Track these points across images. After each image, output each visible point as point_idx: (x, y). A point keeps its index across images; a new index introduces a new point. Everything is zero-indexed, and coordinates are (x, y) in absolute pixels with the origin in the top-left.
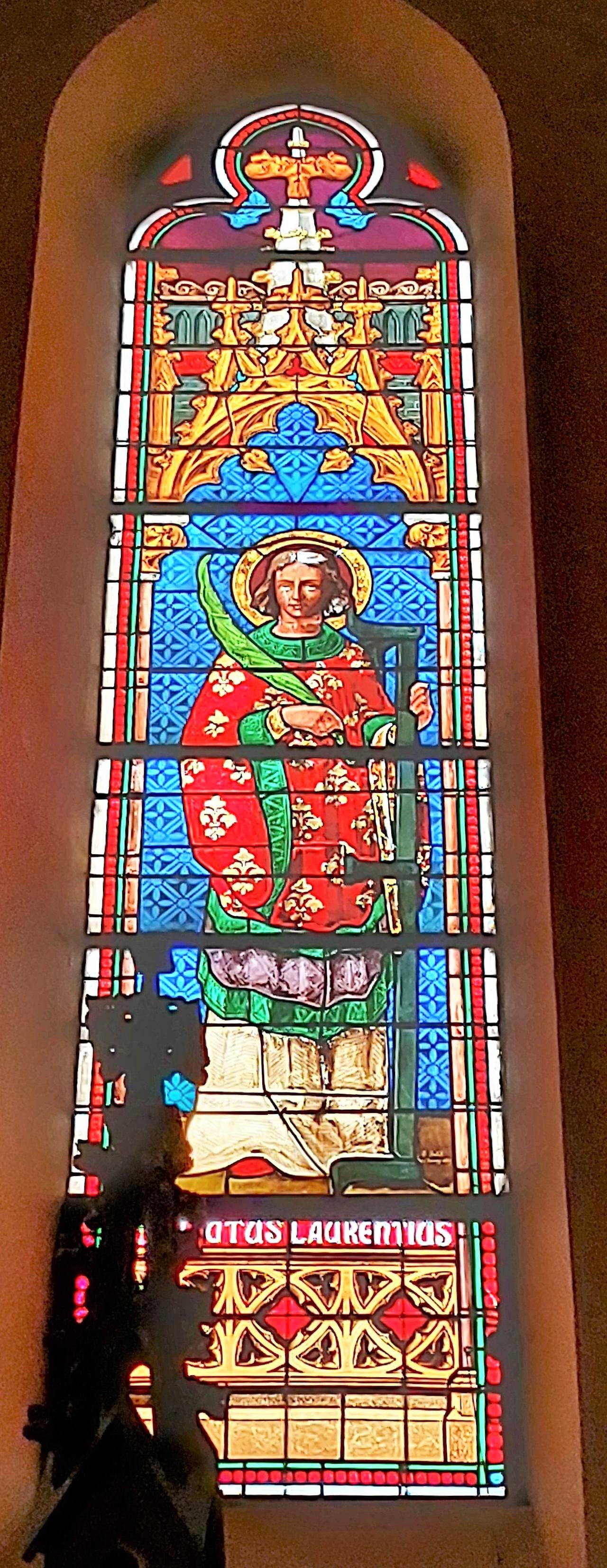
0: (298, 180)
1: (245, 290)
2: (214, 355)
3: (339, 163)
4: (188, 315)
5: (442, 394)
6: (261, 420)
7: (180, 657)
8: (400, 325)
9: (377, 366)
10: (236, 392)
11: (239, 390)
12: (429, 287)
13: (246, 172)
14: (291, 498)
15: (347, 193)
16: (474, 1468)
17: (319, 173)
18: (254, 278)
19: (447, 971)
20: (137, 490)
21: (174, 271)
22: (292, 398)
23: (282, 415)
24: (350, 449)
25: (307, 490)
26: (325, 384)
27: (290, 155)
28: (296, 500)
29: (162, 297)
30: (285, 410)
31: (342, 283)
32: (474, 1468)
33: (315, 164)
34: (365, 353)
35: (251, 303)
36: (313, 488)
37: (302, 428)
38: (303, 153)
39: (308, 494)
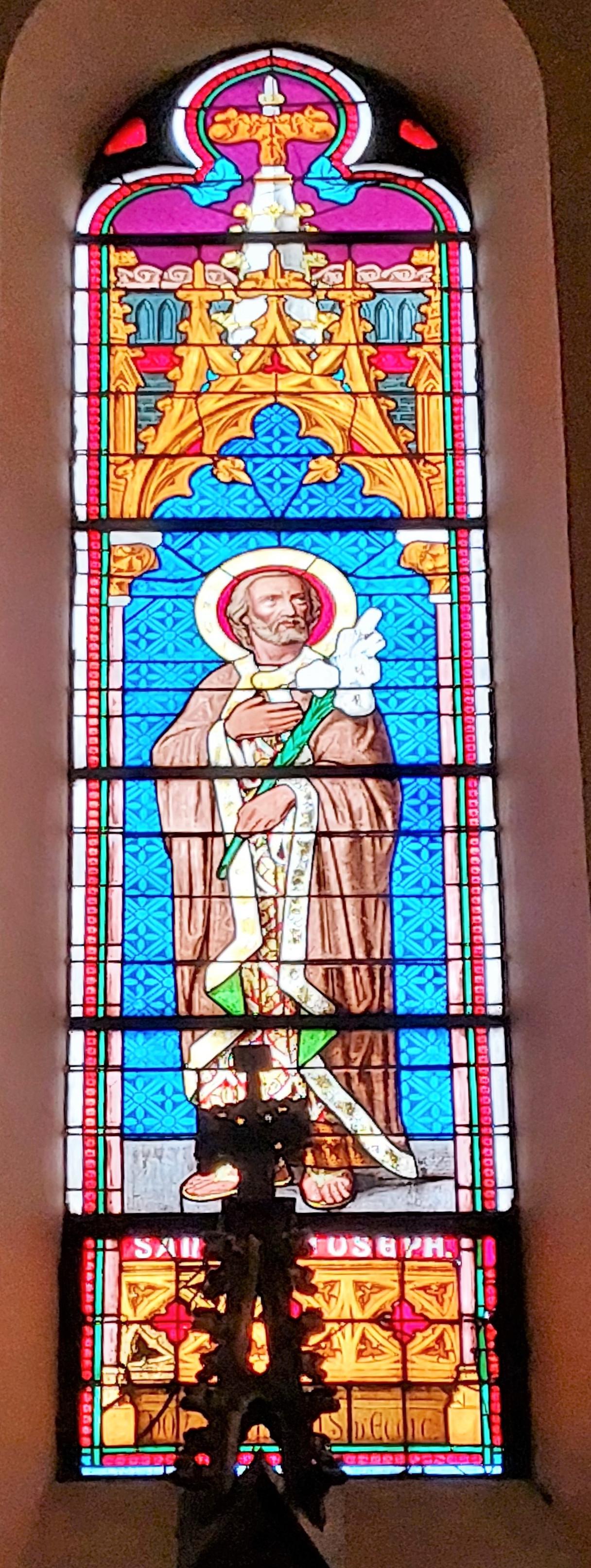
0: (271, 144)
1: (214, 275)
2: (180, 351)
3: (318, 120)
4: (152, 307)
5: (440, 397)
6: (236, 424)
7: (156, 647)
8: (394, 319)
9: (367, 366)
10: (207, 392)
11: (211, 390)
12: (426, 272)
13: (211, 135)
14: (272, 512)
15: (330, 158)
16: (479, 1450)
17: (294, 135)
18: (224, 262)
19: (447, 999)
20: (100, 505)
21: (132, 254)
22: (271, 400)
23: (259, 419)
24: (337, 458)
25: (289, 505)
26: (307, 384)
27: (260, 113)
28: (277, 514)
29: (119, 284)
30: (263, 412)
31: (326, 266)
32: (479, 1450)
33: (291, 124)
34: (353, 351)
35: (223, 291)
36: (296, 502)
37: (283, 433)
38: (277, 110)
39: (291, 509)
